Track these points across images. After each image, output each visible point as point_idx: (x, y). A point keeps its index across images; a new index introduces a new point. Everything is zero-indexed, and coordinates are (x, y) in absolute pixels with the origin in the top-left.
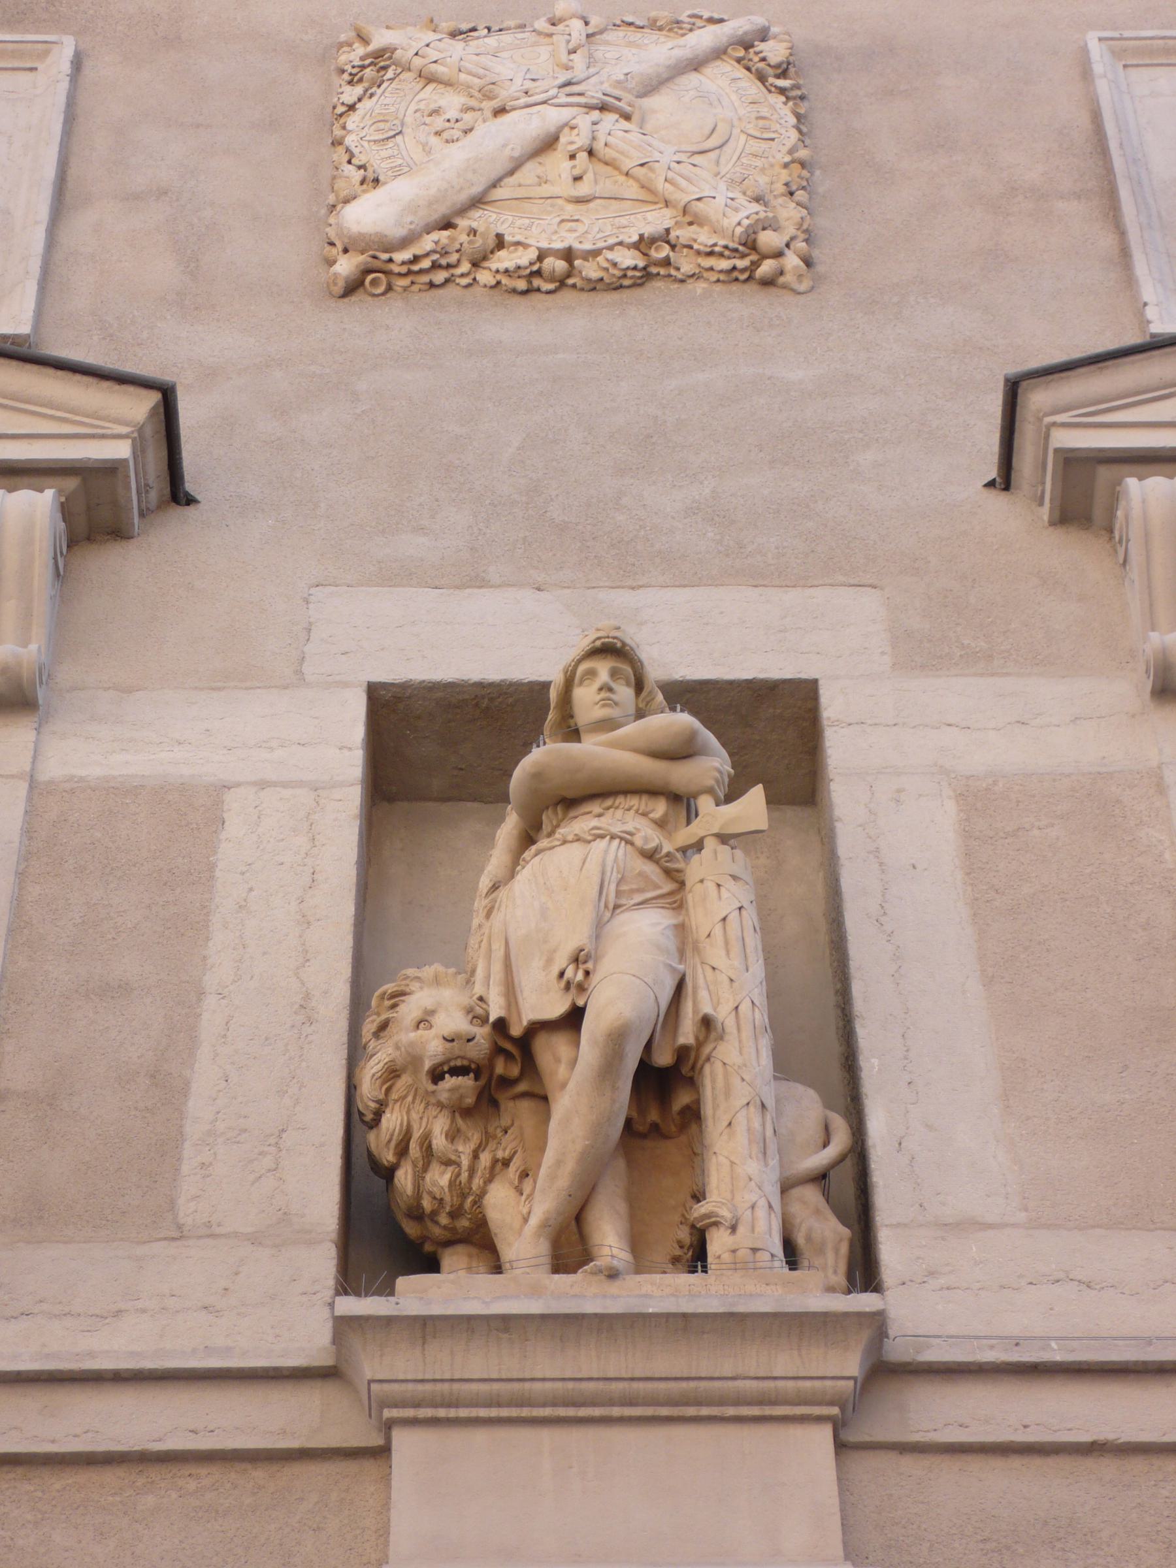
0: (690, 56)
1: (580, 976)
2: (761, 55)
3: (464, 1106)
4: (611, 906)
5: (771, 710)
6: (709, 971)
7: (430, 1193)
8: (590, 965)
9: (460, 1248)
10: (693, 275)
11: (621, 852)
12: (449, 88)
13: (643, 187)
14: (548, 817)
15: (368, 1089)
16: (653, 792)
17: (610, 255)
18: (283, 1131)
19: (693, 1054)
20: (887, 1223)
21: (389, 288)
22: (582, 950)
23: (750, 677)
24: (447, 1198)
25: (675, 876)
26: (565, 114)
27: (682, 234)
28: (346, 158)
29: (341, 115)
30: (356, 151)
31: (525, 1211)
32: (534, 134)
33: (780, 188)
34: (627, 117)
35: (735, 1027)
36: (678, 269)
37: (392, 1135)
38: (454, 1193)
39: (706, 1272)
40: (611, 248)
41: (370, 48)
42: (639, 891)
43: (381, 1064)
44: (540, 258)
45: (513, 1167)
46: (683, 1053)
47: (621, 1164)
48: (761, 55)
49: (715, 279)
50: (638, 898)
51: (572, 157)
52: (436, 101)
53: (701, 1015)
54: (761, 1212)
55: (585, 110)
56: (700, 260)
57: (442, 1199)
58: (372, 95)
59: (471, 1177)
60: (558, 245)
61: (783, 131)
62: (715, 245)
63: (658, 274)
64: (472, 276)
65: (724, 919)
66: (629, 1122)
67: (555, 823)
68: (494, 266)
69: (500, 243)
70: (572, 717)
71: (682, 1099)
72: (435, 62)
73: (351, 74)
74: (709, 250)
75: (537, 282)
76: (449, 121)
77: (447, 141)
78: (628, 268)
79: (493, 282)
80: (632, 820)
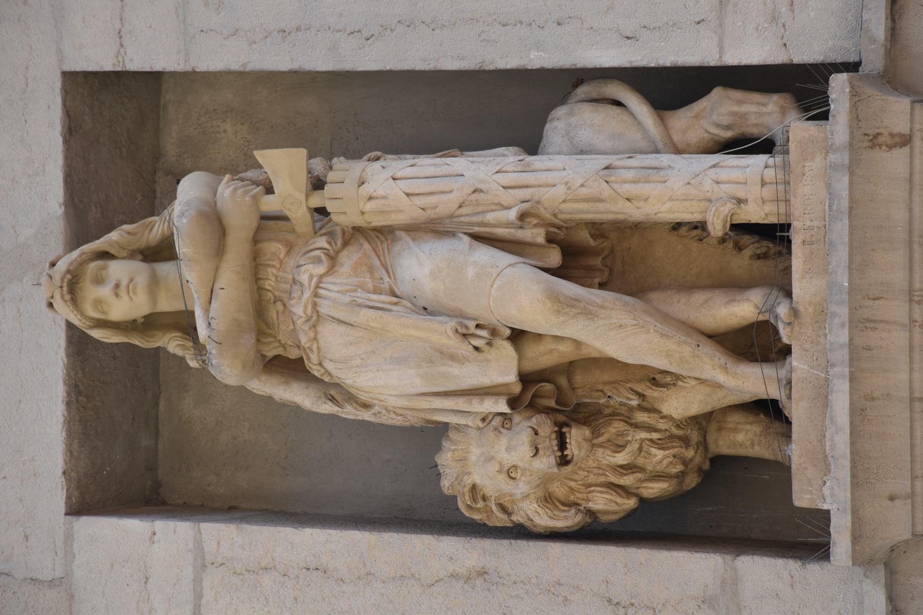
1: (484, 333)
4: (395, 300)
5: (86, 118)
6: (463, 211)
8: (472, 324)
11: (332, 287)
14: (269, 351)
15: (566, 521)
18: (609, 601)
19: (552, 229)
20: (718, 57)
22: (457, 331)
23: (61, 140)
31: (694, 383)
35: (525, 190)
37: (611, 500)
38: (670, 445)
43: (539, 510)
47: (654, 296)
54: (723, 174)
59: (656, 430)
65: (408, 195)
67: (278, 344)
70: (135, 321)
71: (584, 237)
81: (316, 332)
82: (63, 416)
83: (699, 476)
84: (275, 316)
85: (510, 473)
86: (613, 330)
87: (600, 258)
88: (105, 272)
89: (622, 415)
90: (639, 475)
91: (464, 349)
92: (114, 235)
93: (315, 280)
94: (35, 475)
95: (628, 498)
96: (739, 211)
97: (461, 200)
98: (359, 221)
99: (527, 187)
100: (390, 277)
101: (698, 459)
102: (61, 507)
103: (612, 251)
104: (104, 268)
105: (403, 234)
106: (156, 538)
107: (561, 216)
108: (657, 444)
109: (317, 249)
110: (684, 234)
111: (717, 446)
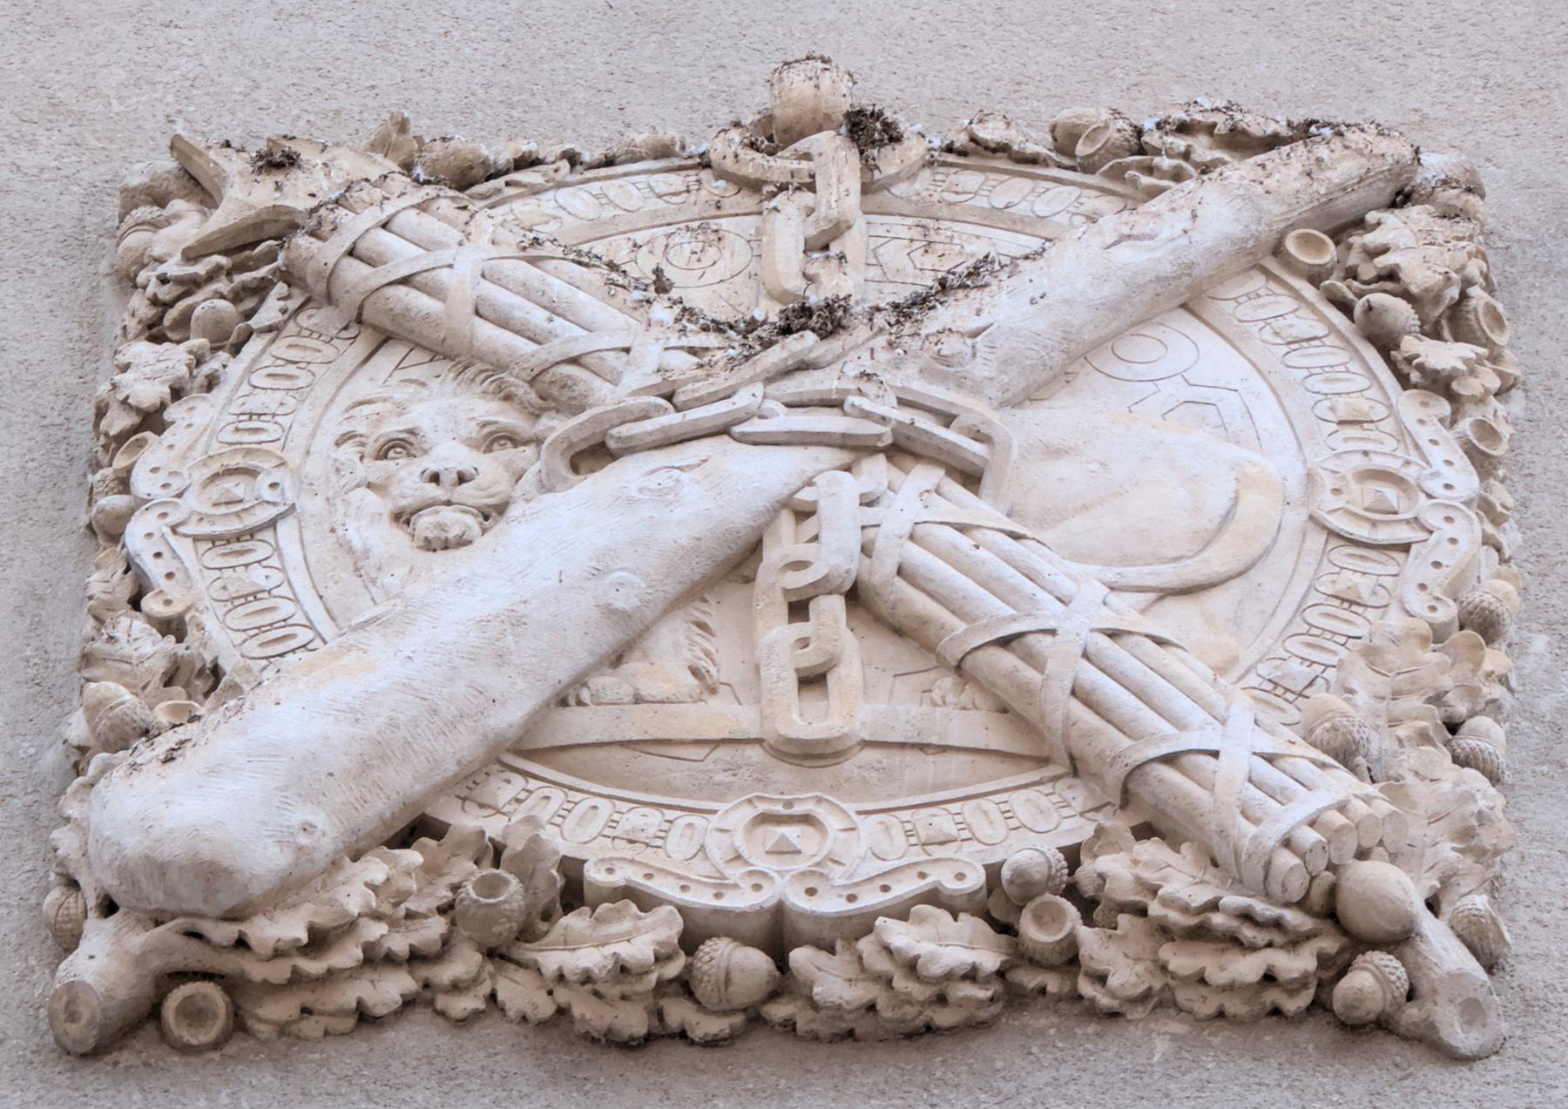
0: (1167, 269)
2: (1383, 261)
10: (1145, 997)
12: (442, 367)
13: (1004, 710)
17: (900, 935)
21: (238, 1025)
26: (775, 471)
27: (1118, 868)
28: (125, 591)
29: (122, 438)
30: (155, 570)
32: (684, 536)
33: (1419, 713)
34: (971, 478)
36: (1101, 979)
40: (901, 912)
41: (221, 219)
44: (690, 941)
48: (1383, 261)
49: (1209, 1008)
51: (798, 609)
52: (401, 409)
55: (843, 457)
56: (1167, 952)
58: (211, 383)
60: (742, 900)
61: (1433, 518)
62: (1214, 906)
63: (1042, 991)
64: (486, 989)
68: (552, 960)
69: (573, 892)
72: (405, 281)
73: (155, 301)
74: (1192, 921)
75: (678, 1012)
76: (435, 478)
77: (429, 546)
78: (949, 976)
79: (546, 1009)
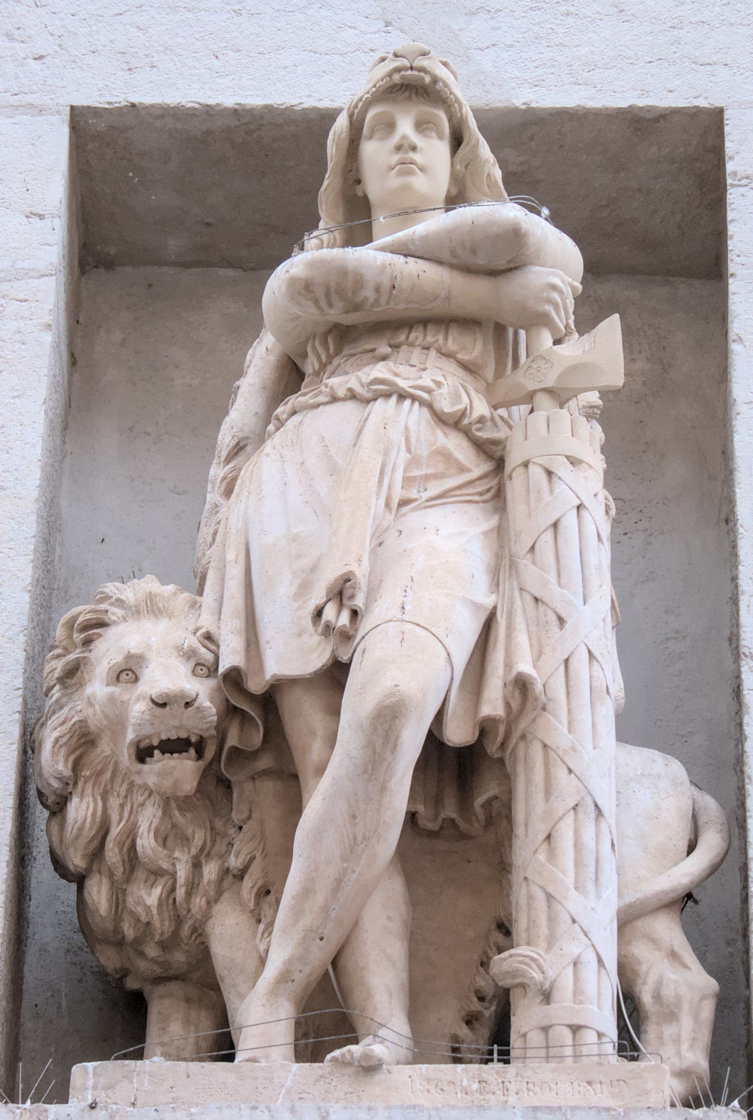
1: (344, 619)
3: (181, 794)
5: (654, 149)
7: (133, 914)
9: (173, 987)
15: (52, 762)
16: (467, 323)
19: (502, 730)
23: (624, 104)
24: (157, 924)
25: (494, 455)
38: (166, 916)
39: (507, 1062)
42: (435, 476)
43: (69, 725)
45: (248, 882)
46: (485, 729)
50: (434, 489)
53: (514, 673)
57: (148, 924)
59: (189, 894)
65: (555, 525)
66: (412, 817)
70: (359, 182)
71: (487, 790)
80: (432, 373)
81: (344, 400)
82: (218, 105)
83: (117, 971)
84: (369, 346)
85: (128, 672)
86: (350, 806)
87: (454, 815)
88: (434, 134)
89: (213, 845)
90: (119, 872)
91: (318, 596)
92: (485, 151)
93: (425, 396)
94: (130, 70)
95: (84, 856)
96: (530, 994)
97: (546, 599)
98: (513, 460)
99: (568, 693)
100: (427, 501)
101: (142, 965)
102: (83, 100)
103: (464, 836)
104: (440, 137)
105: (494, 521)
106: (35, 220)
107: (522, 745)
108: (168, 897)
109: (471, 401)
110: (492, 940)
111: (162, 997)
